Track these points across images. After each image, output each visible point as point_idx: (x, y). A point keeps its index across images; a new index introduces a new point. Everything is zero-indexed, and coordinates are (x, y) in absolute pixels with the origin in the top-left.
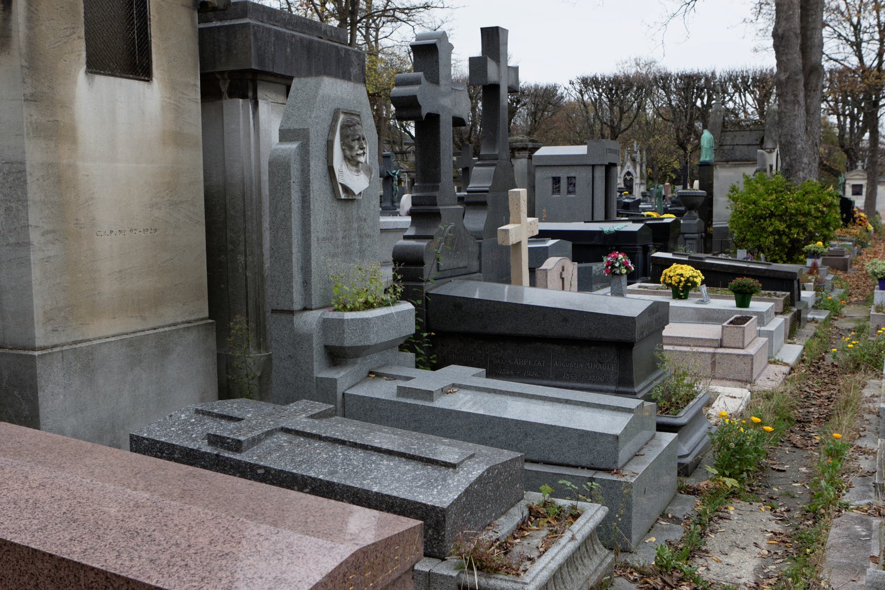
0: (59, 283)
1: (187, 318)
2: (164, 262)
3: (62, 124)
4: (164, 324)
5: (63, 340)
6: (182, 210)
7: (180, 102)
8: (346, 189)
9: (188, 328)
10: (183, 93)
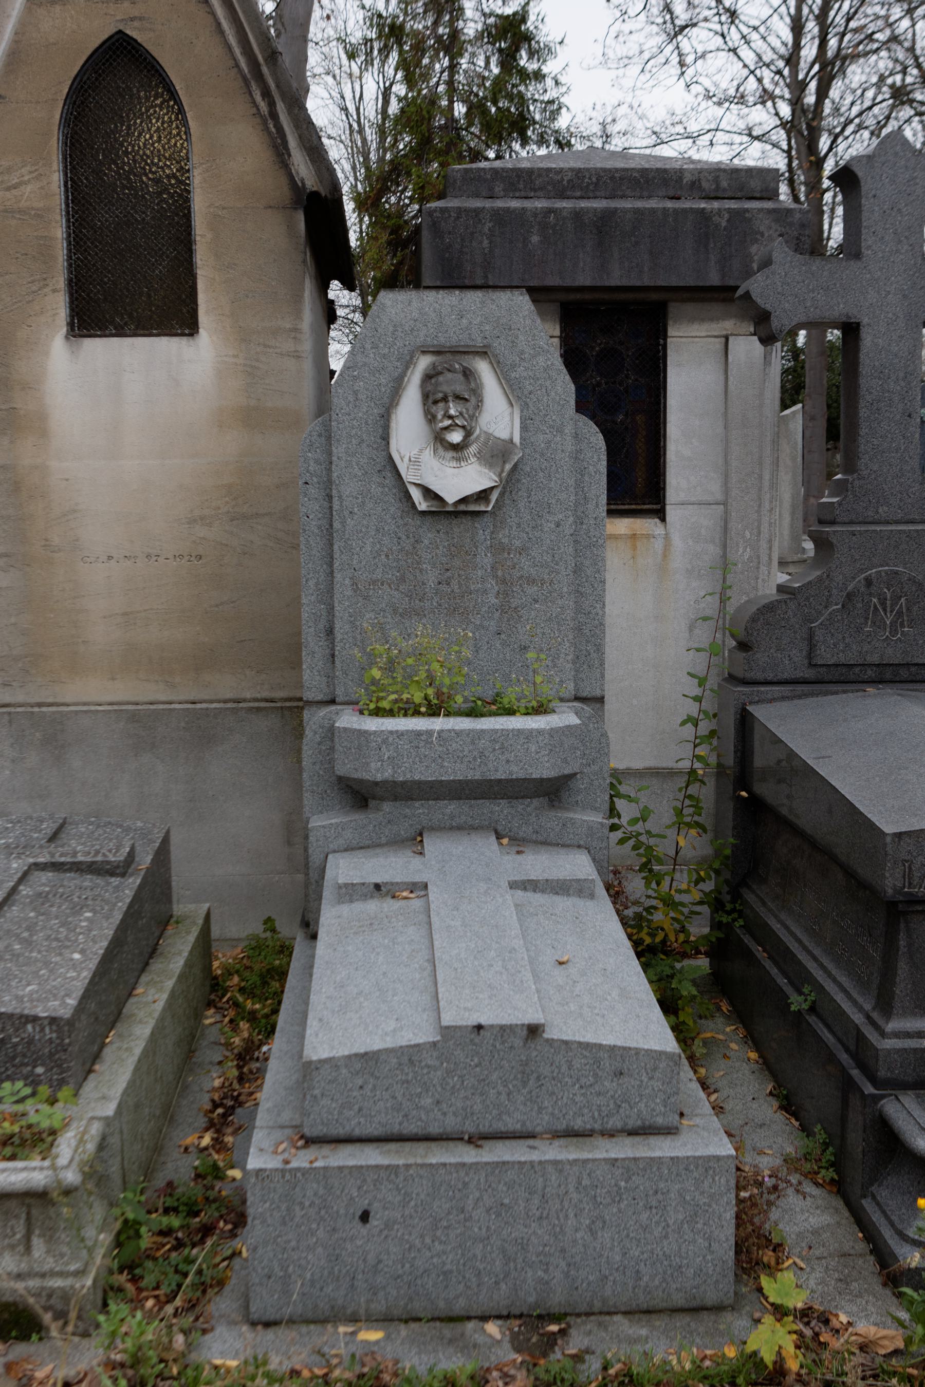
0: (15, 624)
1: (266, 694)
2: (217, 606)
3: (22, 412)
4: (213, 697)
5: (20, 698)
6: (260, 527)
7: (257, 360)
8: (428, 493)
9: (258, 709)
10: (265, 346)
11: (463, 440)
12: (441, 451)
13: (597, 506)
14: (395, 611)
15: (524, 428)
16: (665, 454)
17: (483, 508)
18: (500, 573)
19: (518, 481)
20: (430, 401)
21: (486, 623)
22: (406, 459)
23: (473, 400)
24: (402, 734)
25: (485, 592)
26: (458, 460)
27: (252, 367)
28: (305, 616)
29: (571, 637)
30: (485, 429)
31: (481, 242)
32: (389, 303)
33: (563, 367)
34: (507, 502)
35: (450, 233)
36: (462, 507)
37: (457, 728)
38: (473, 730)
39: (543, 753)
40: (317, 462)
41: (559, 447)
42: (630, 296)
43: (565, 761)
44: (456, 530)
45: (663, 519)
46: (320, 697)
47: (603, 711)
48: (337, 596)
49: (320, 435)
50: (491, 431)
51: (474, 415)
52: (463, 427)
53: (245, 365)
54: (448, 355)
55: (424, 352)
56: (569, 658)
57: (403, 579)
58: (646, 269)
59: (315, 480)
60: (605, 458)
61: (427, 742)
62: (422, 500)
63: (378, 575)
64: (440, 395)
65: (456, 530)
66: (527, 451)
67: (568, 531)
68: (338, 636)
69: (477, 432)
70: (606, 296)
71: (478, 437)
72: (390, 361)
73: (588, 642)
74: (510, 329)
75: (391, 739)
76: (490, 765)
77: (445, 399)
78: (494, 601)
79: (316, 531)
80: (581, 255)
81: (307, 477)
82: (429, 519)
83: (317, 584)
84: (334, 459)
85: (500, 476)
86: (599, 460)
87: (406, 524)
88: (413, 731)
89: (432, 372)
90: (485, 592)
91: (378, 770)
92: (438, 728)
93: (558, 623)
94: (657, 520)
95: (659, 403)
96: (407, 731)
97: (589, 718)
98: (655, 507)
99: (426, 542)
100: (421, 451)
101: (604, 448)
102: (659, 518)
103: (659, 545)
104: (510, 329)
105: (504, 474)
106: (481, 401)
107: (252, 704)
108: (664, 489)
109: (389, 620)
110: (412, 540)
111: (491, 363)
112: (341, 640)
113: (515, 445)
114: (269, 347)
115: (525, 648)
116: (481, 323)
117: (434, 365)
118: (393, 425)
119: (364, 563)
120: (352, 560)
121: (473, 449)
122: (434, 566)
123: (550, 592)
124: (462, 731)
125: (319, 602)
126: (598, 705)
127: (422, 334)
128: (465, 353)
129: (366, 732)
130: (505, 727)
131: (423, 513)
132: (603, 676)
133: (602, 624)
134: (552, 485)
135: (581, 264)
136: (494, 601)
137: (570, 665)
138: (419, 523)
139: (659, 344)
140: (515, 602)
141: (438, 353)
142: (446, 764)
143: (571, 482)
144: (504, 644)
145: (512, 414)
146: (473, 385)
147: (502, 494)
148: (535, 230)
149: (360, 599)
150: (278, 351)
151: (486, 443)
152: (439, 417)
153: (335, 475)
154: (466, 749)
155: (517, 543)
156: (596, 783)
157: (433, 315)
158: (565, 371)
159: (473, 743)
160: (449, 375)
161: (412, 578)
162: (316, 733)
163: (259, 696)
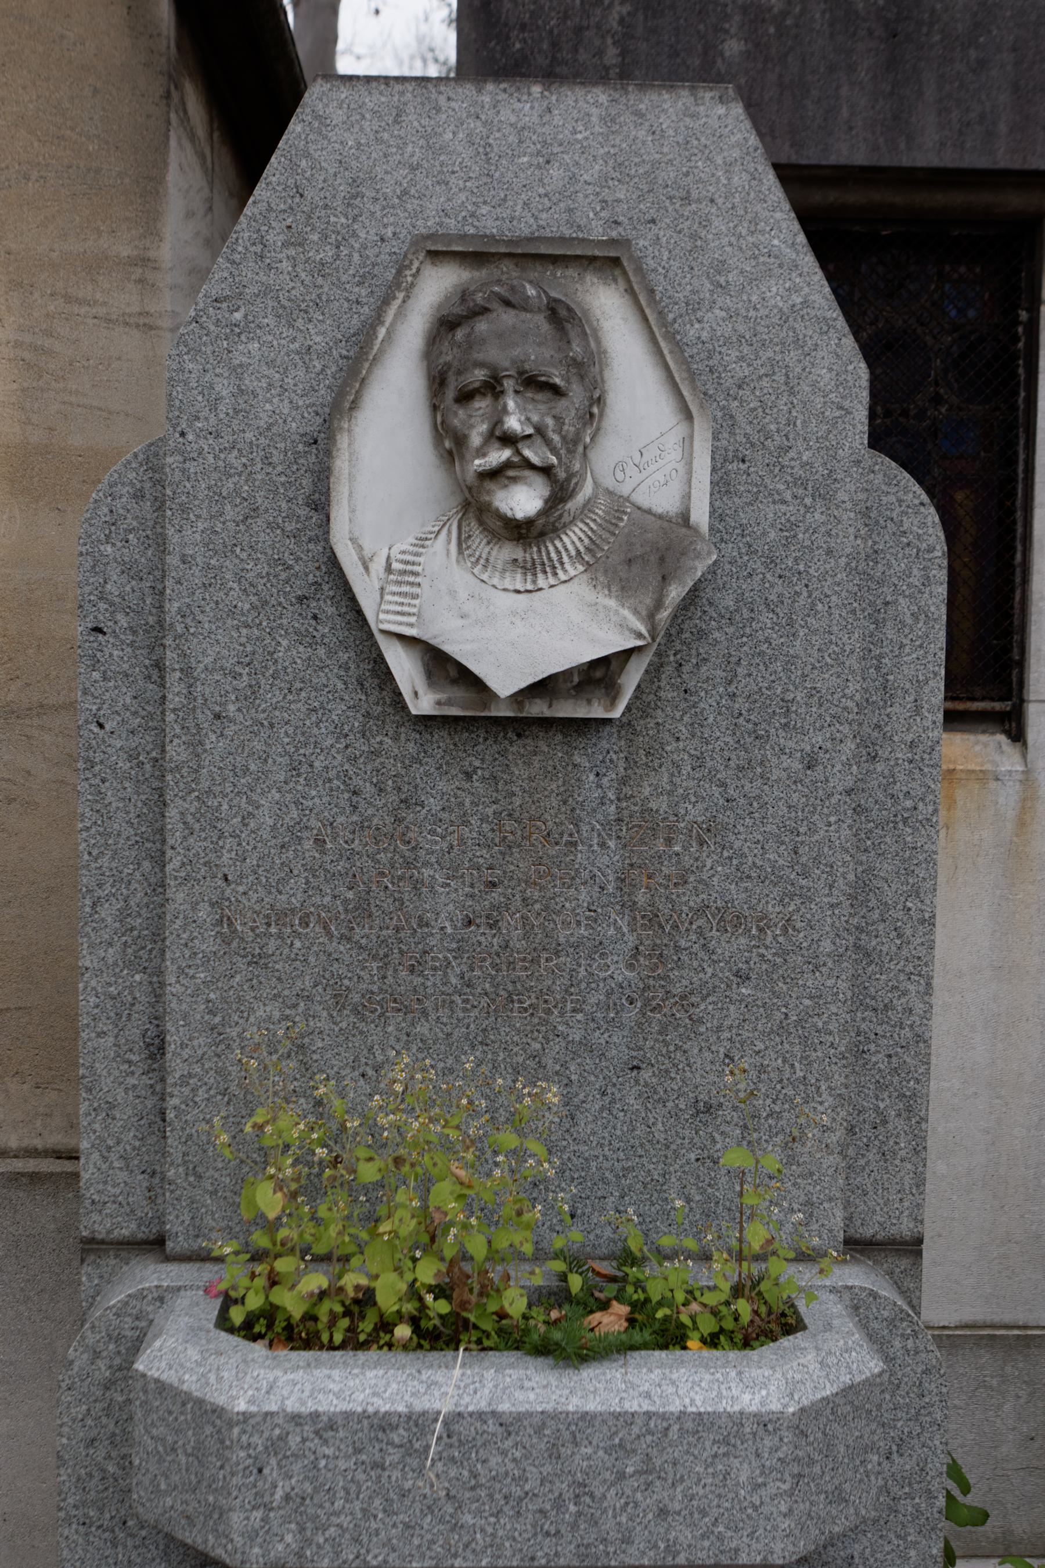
7: (49, 333)
9: (35, 1178)
10: (69, 299)
11: (544, 512)
12: (479, 543)
13: (918, 710)
14: (340, 999)
15: (721, 486)
16: (1026, 580)
17: (597, 711)
18: (641, 897)
19: (701, 634)
20: (450, 394)
21: (598, 1038)
22: (378, 566)
23: (577, 394)
24: (332, 1426)
25: (599, 948)
26: (530, 569)
27: (35, 348)
28: (87, 1003)
29: (838, 1080)
30: (609, 482)
31: (600, 53)
32: (338, 116)
33: (835, 313)
34: (667, 694)
35: (523, 27)
36: (538, 708)
37: (505, 1407)
38: (555, 1416)
39: (772, 1489)
40: (128, 570)
41: (820, 539)
42: (957, 199)
43: (838, 1497)
44: (519, 771)
45: (1018, 735)
46: (126, 1231)
47: (918, 1277)
48: (174, 957)
49: (139, 496)
50: (625, 490)
51: (577, 440)
52: (546, 471)
53: (18, 345)
54: (506, 266)
55: (435, 256)
56: (833, 1138)
57: (362, 910)
58: (1003, 128)
59: (123, 621)
60: (943, 575)
61: (407, 1449)
62: (421, 685)
63: (293, 895)
64: (479, 375)
65: (519, 771)
66: (728, 549)
67: (839, 782)
68: (176, 1066)
69: (587, 490)
70: (896, 198)
71: (588, 505)
72: (339, 284)
73: (881, 1086)
74: (687, 199)
75: (294, 1441)
76: (608, 1524)
77: (493, 388)
78: (624, 974)
79: (124, 765)
80: (844, 91)
81: (101, 614)
82: (441, 739)
83: (123, 915)
84: (173, 560)
85: (650, 618)
86: (927, 581)
87: (375, 753)
88: (364, 1415)
89: (458, 310)
90: (599, 948)
91: (251, 1536)
92: (446, 1407)
93: (804, 1040)
94: (1002, 738)
95: (1013, 462)
96: (348, 1415)
97: (891, 1322)
98: (998, 706)
99: (433, 804)
100: (422, 542)
101: (941, 548)
102: (1008, 734)
103: (1008, 796)
104: (687, 199)
105: (664, 615)
106: (600, 401)
107: (19, 1165)
108: (1021, 664)
109: (323, 1024)
110: (393, 798)
111: (630, 291)
112: (184, 1080)
113: (695, 530)
114: (80, 302)
115: (708, 1108)
116: (604, 181)
117: (464, 295)
118: (341, 464)
119: (252, 861)
120: (218, 851)
121: (573, 538)
122: (453, 873)
123: (783, 953)
124: (519, 1418)
125: (128, 965)
126: (905, 1263)
127: (432, 207)
128: (555, 260)
129: (218, 1411)
130: (657, 1407)
131: (426, 721)
132: (920, 1182)
133: (921, 1039)
134: (798, 647)
135: (845, 112)
136: (624, 974)
137: (834, 1159)
138: (412, 749)
139: (1016, 322)
140: (682, 981)
141: (475, 258)
142: (468, 1519)
143: (853, 641)
144: (649, 1095)
145: (688, 441)
146: (577, 349)
147: (654, 672)
148: (733, 26)
149: (241, 963)
150: (101, 311)
151: (610, 524)
152: (476, 439)
153: (173, 608)
154: (532, 1472)
155: (695, 812)
156: (906, 1506)
157: (467, 153)
158: (841, 323)
159: (554, 1453)
160: (507, 317)
161: (389, 905)
162: (96, 1355)
163: (38, 1143)
